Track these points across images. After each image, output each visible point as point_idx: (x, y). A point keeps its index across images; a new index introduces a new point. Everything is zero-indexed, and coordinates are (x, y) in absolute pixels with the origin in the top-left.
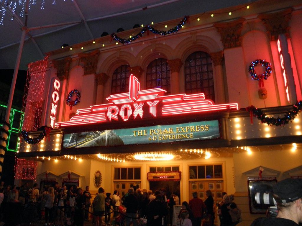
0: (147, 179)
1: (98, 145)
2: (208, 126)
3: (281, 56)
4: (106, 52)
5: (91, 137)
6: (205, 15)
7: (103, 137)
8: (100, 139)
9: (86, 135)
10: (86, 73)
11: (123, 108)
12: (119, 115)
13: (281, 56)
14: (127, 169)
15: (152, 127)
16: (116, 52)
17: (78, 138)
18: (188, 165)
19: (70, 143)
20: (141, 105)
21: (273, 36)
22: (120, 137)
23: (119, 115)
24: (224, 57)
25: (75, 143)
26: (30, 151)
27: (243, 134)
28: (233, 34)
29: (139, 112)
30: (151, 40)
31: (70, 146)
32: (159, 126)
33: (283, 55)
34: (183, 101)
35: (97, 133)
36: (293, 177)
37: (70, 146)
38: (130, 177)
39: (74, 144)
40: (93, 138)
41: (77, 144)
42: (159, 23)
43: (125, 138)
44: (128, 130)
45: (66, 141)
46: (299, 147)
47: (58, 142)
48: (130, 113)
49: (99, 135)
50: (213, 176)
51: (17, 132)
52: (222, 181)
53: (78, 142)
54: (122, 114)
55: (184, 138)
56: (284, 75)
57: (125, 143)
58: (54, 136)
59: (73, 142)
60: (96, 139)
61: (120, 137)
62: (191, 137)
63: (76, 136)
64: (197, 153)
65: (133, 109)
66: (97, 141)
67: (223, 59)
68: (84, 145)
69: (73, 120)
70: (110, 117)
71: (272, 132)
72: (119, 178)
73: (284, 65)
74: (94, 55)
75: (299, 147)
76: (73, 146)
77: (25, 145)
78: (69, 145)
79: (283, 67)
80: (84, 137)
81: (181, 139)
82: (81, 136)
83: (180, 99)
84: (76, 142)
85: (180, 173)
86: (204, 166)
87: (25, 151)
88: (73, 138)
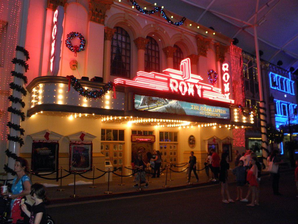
0: (131, 141)
1: (168, 112)
2: (226, 111)
3: (55, 27)
4: (116, 8)
5: (161, 103)
6: (195, 25)
7: (172, 105)
8: (169, 106)
9: (157, 101)
11: (181, 83)
12: (178, 89)
13: (55, 27)
14: (106, 130)
15: (202, 105)
16: (123, 12)
17: (150, 102)
18: (132, 129)
19: (141, 105)
21: (52, 4)
22: (183, 108)
23: (178, 89)
25: (147, 106)
26: (43, 102)
27: (111, 105)
28: (101, 10)
29: (191, 91)
30: (156, 21)
31: (142, 109)
32: (205, 105)
33: (57, 26)
34: (212, 91)
35: (166, 101)
36: (35, 141)
37: (142, 109)
38: (115, 139)
39: (145, 107)
40: (164, 105)
41: (149, 107)
42: (168, 10)
43: (187, 109)
44: (188, 103)
45: (137, 102)
47: (107, 100)
49: (168, 103)
50: (161, 139)
52: (177, 144)
53: (149, 106)
54: (181, 88)
55: (217, 116)
56: (53, 45)
57: (187, 114)
58: (56, 85)
59: (145, 105)
60: (166, 106)
61: (183, 108)
62: (219, 116)
63: (147, 99)
64: (109, 117)
66: (167, 108)
68: (156, 110)
69: (137, 80)
70: (172, 89)
71: (89, 103)
72: (104, 140)
73: (56, 36)
74: (129, 12)
76: (145, 109)
77: (242, 117)
79: (54, 38)
80: (155, 101)
81: (215, 117)
82: (152, 100)
83: (210, 89)
84: (148, 105)
85: (154, 136)
86: (111, 130)
87: (103, 107)
88: (144, 100)
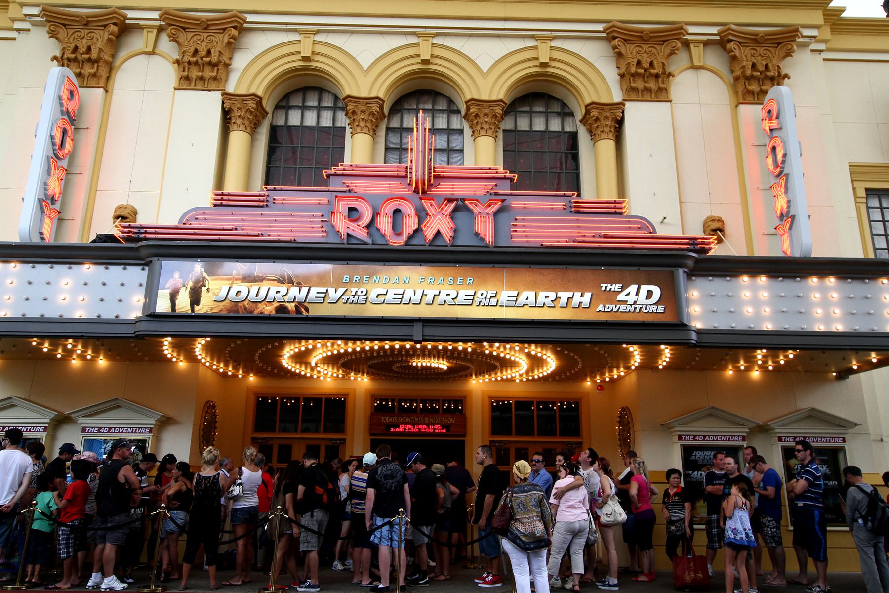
10: (186, 82)
14: (464, 439)
24: (623, 118)
46: (672, 356)
48: (410, 224)
51: (505, 570)
65: (422, 215)
67: (619, 124)
75: (672, 356)
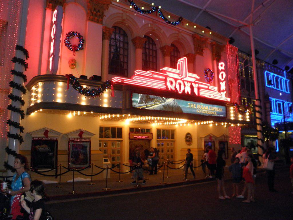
0: (128, 139)
1: (165, 110)
2: (222, 109)
3: (54, 26)
4: (114, 7)
5: (158, 101)
6: (192, 25)
7: (169, 104)
8: (166, 104)
9: (154, 99)
12: (175, 87)
13: (54, 26)
14: (104, 128)
15: (198, 103)
16: (121, 12)
17: (148, 100)
18: (129, 127)
19: (139, 103)
20: (189, 84)
21: (51, 4)
22: (180, 106)
23: (175, 87)
25: (145, 104)
27: (109, 103)
28: (99, 10)
29: (188, 90)
30: (154, 20)
31: (140, 107)
32: (202, 103)
33: (56, 26)
34: (208, 89)
35: (163, 99)
36: (34, 138)
37: (140, 107)
38: (113, 136)
39: (143, 105)
40: (161, 103)
41: (146, 105)
42: (165, 10)
43: (183, 108)
44: (185, 102)
45: (134, 100)
47: (105, 98)
49: (165, 101)
50: (158, 136)
52: (174, 141)
53: (147, 104)
54: (178, 87)
55: (213, 114)
56: (52, 44)
57: (184, 112)
58: (55, 83)
59: (142, 103)
60: (163, 104)
61: (180, 106)
62: (215, 114)
63: (144, 97)
64: (108, 115)
66: (164, 106)
68: (153, 108)
69: (135, 79)
70: (169, 87)
71: (88, 101)
72: (102, 137)
73: (55, 35)
74: (127, 12)
76: (143, 107)
78: (138, 105)
79: (53, 37)
80: (152, 100)
81: (212, 114)
82: (150, 98)
83: (207, 87)
84: (145, 103)
85: (152, 134)
86: (110, 127)
87: (102, 105)
88: (142, 98)
